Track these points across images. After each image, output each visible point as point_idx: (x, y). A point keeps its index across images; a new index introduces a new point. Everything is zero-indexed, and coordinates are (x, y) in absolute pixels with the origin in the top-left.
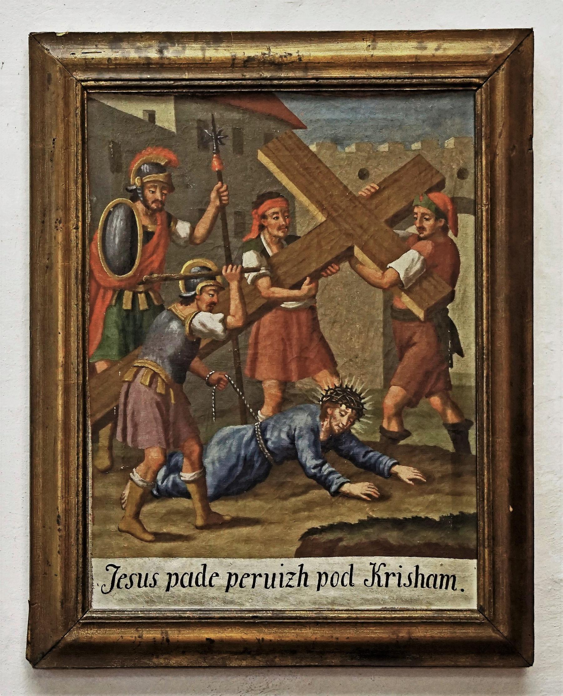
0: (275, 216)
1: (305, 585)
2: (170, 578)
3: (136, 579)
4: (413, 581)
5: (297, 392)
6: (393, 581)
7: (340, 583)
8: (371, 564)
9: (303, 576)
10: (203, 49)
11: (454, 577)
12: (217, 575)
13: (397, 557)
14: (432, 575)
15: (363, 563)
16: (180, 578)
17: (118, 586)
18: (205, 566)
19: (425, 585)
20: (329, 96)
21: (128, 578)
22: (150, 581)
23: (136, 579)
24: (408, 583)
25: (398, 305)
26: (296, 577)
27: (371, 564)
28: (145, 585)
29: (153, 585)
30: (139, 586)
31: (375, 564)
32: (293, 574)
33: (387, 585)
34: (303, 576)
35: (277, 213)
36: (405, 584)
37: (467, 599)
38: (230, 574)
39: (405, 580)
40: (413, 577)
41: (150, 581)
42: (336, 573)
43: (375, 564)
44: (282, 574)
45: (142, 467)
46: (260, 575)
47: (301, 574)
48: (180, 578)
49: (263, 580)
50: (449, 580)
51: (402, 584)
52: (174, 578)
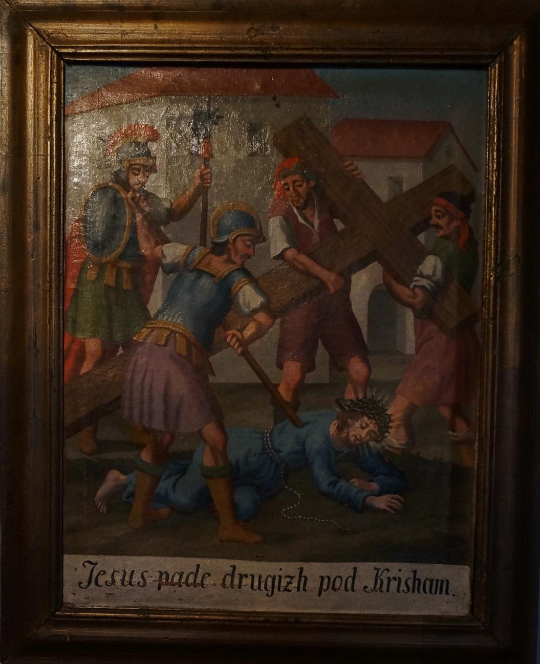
1: (304, 590)
2: (161, 577)
4: (411, 588)
6: (394, 584)
7: (343, 587)
8: (375, 569)
9: (303, 579)
10: (515, 118)
12: (209, 575)
13: (73, 556)
14: (270, 576)
15: (366, 570)
16: (332, 581)
17: (97, 584)
18: (198, 566)
19: (301, 589)
20: (66, 252)
22: (137, 579)
24: (405, 589)
26: (296, 580)
27: (375, 569)
29: (406, 591)
31: (379, 569)
32: (292, 578)
33: (388, 590)
34: (303, 579)
36: (403, 591)
38: (160, 572)
41: (137, 579)
43: (379, 569)
44: (280, 577)
46: (395, 579)
47: (415, 579)
48: (332, 581)
49: (249, 581)
50: (441, 587)
51: (401, 590)
52: (326, 581)
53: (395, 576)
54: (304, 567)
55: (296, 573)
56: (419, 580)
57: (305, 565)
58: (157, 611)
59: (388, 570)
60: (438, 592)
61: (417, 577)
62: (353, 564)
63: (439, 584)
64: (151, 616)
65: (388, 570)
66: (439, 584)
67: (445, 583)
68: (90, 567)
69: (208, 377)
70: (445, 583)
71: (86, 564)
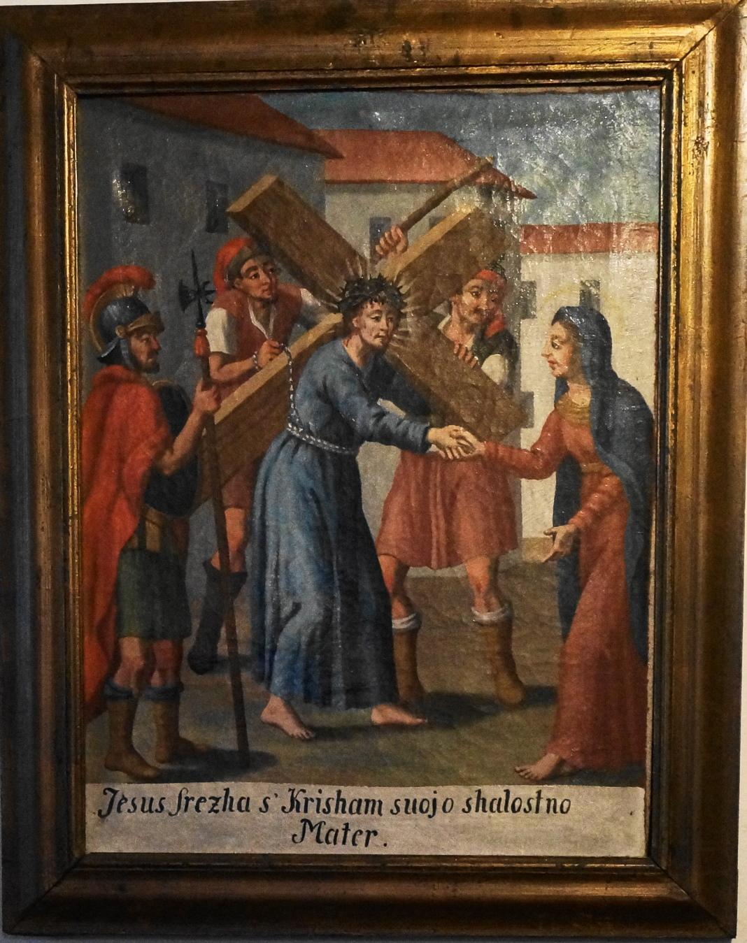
0: (252, 273)
3: (139, 804)
5: (507, 454)
9: (341, 803)
11: (380, 802)
21: (129, 802)
22: (156, 806)
23: (139, 804)
25: (292, 440)
26: (221, 802)
27: (290, 790)
28: (150, 811)
29: (527, 809)
30: (343, 812)
31: (293, 790)
32: (217, 799)
35: (255, 268)
37: (629, 838)
39: (323, 806)
40: (534, 803)
41: (156, 806)
42: (426, 799)
45: (479, 600)
47: (339, 799)
53: (368, 798)
54: (511, 790)
55: (535, 795)
56: (344, 801)
57: (342, 788)
58: (593, 859)
59: (304, 791)
60: (481, 808)
61: (342, 797)
62: (337, 788)
63: (228, 806)
64: (589, 865)
65: (304, 791)
66: (228, 806)
67: (377, 804)
68: (110, 794)
69: (551, 474)
70: (377, 804)
71: (107, 791)
